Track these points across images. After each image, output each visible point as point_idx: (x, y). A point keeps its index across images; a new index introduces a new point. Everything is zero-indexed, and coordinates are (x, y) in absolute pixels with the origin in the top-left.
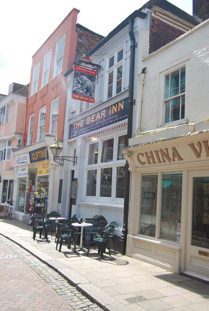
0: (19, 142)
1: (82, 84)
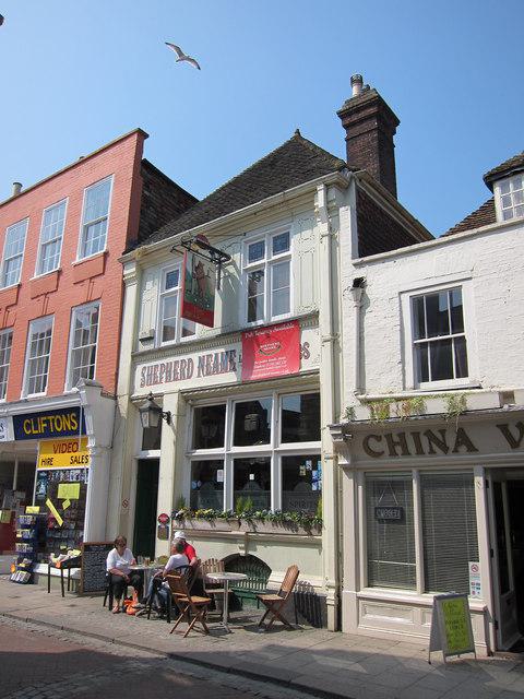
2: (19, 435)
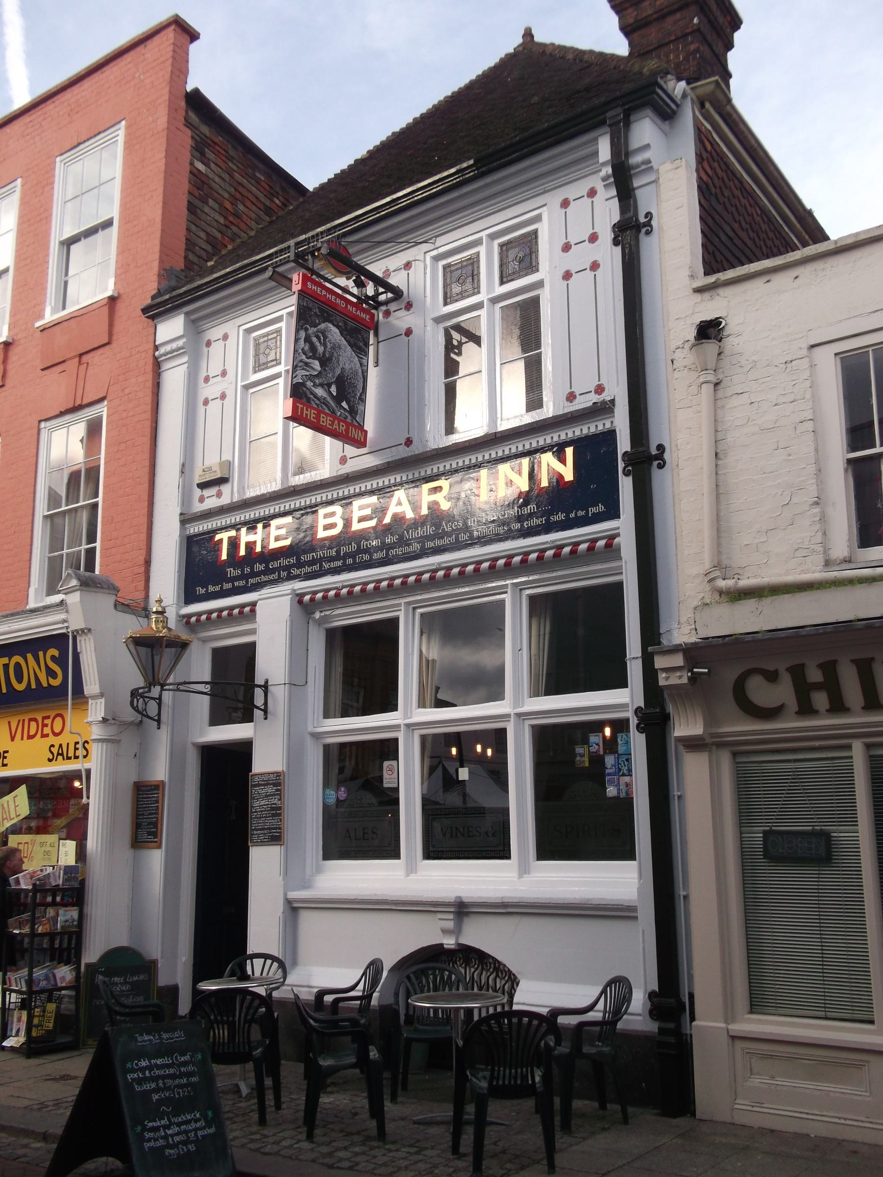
1: (325, 362)
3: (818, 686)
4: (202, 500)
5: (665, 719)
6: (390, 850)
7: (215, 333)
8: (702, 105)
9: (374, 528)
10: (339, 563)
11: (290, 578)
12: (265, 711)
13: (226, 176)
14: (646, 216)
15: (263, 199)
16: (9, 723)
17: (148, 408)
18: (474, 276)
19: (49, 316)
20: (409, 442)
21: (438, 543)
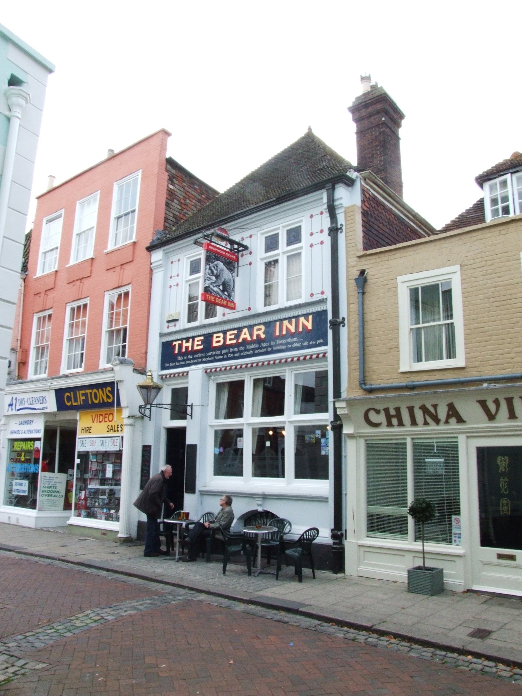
0: (9, 366)
1: (217, 277)
2: (61, 406)
3: (394, 416)
4: (168, 327)
5: (340, 427)
6: (240, 473)
7: (175, 258)
8: (365, 180)
9: (235, 344)
10: (221, 357)
11: (203, 362)
12: (191, 416)
13: (182, 189)
14: (341, 225)
15: (197, 196)
16: (92, 416)
17: (148, 288)
18: (277, 242)
19: (111, 247)
20: (249, 309)
21: (260, 351)
